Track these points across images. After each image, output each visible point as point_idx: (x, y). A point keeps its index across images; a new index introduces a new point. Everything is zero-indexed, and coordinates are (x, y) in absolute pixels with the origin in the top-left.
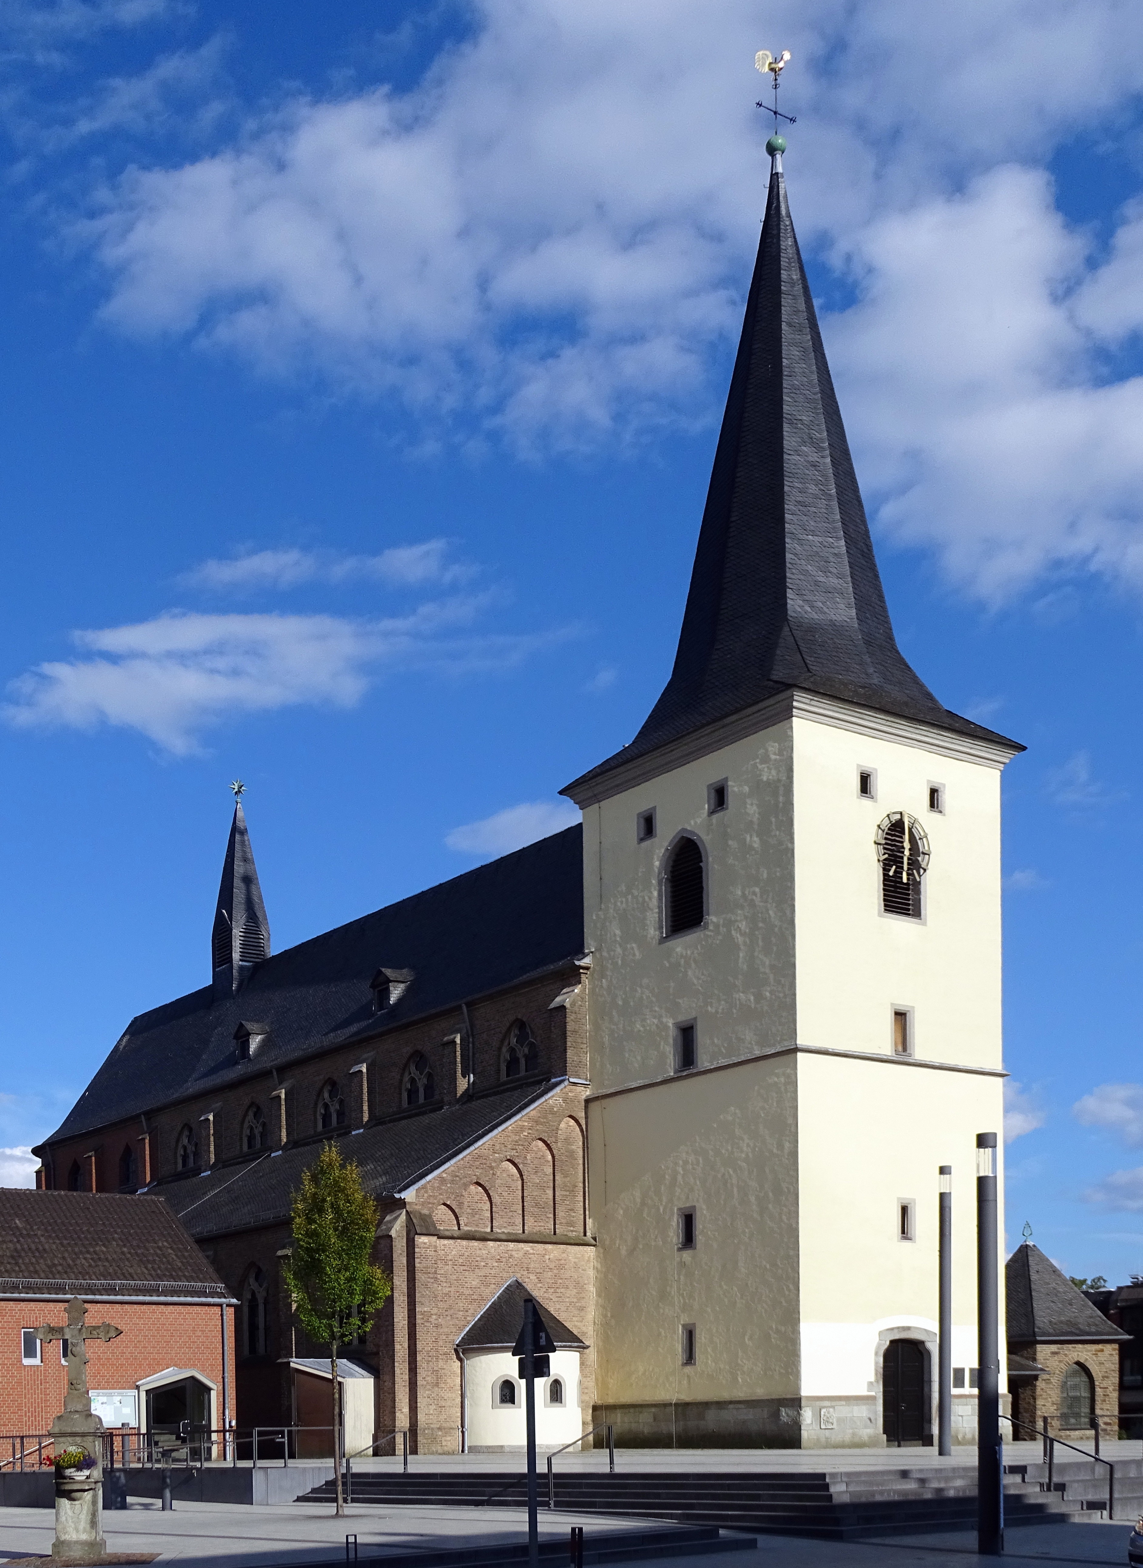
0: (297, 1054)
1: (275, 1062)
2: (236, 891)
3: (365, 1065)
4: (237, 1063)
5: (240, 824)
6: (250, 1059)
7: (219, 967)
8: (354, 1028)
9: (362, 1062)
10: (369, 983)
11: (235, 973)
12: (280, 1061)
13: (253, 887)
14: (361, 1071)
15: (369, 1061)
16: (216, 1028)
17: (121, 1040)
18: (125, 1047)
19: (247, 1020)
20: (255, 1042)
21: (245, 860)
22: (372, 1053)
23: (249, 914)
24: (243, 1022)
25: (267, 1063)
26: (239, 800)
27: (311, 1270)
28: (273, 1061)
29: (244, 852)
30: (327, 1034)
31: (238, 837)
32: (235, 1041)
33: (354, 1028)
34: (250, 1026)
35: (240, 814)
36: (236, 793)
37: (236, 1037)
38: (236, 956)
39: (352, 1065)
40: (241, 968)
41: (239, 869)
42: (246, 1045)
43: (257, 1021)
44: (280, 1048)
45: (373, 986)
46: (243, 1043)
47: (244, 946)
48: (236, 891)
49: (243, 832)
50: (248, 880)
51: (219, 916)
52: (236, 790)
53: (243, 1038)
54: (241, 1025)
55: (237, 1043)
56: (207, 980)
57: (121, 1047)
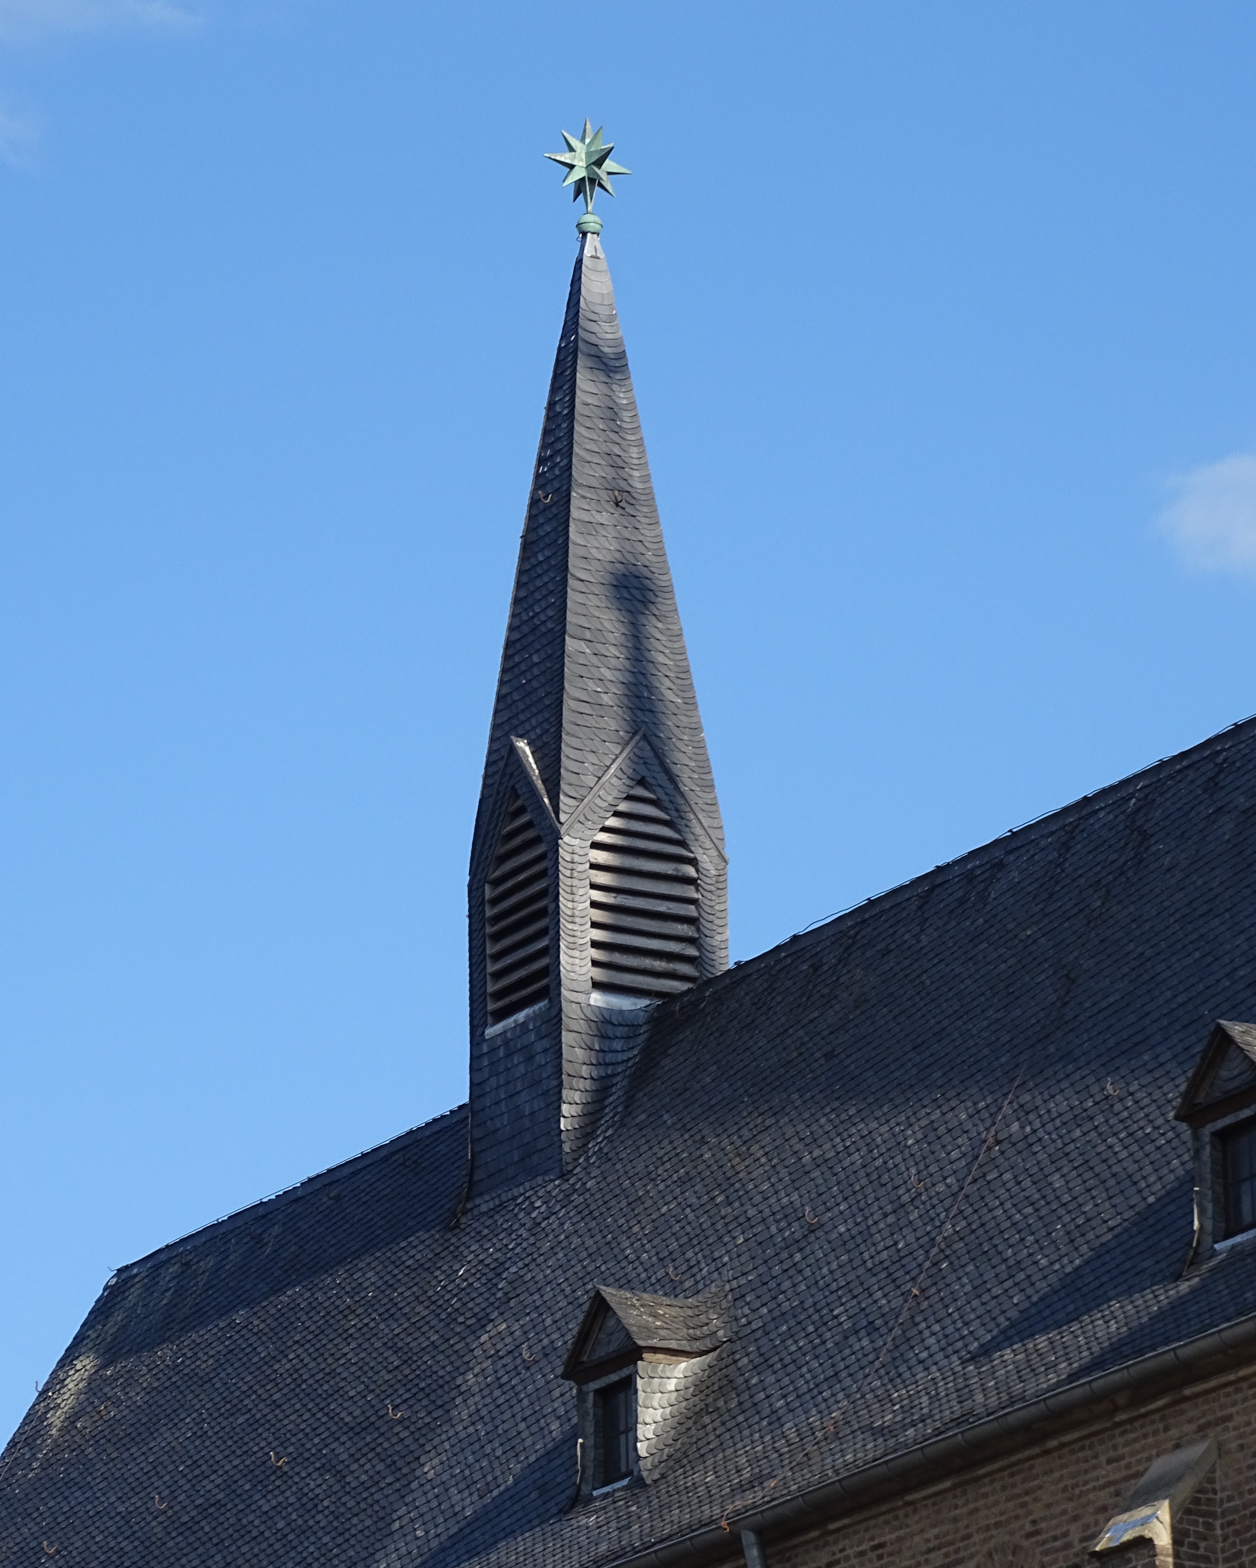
0: (857, 1454)
1: (749, 1498)
2: (572, 632)
3: (1164, 1511)
4: (577, 1501)
5: (601, 332)
6: (639, 1483)
7: (500, 1015)
8: (1107, 1324)
9: (1148, 1496)
10: (1174, 1092)
11: (576, 1050)
12: (786, 1485)
13: (654, 628)
14: (1144, 1543)
15: (1186, 1488)
16: (483, 1322)
17: (55, 1382)
18: (72, 1418)
19: (626, 1284)
20: (661, 1394)
21: (623, 499)
22: (1199, 1449)
23: (638, 760)
24: (609, 1293)
25: (716, 1499)
26: (592, 221)
27: (887, 1522)
28: (742, 1488)
29: (618, 464)
30: (986, 1351)
31: (586, 383)
32: (571, 1388)
33: (1107, 1324)
34: (639, 1313)
35: (597, 286)
36: (579, 187)
37: (576, 1369)
38: (577, 963)
39: (1107, 1512)
40: (605, 1026)
41: (593, 543)
42: (614, 1407)
43: (672, 1289)
44: (776, 1420)
45: (1192, 1113)
46: (603, 1394)
47: (620, 913)
48: (572, 632)
49: (612, 366)
50: (636, 592)
51: (501, 768)
52: (579, 173)
53: (605, 1367)
54: (600, 1308)
55: (581, 1396)
56: (445, 1087)
57: (56, 1419)
